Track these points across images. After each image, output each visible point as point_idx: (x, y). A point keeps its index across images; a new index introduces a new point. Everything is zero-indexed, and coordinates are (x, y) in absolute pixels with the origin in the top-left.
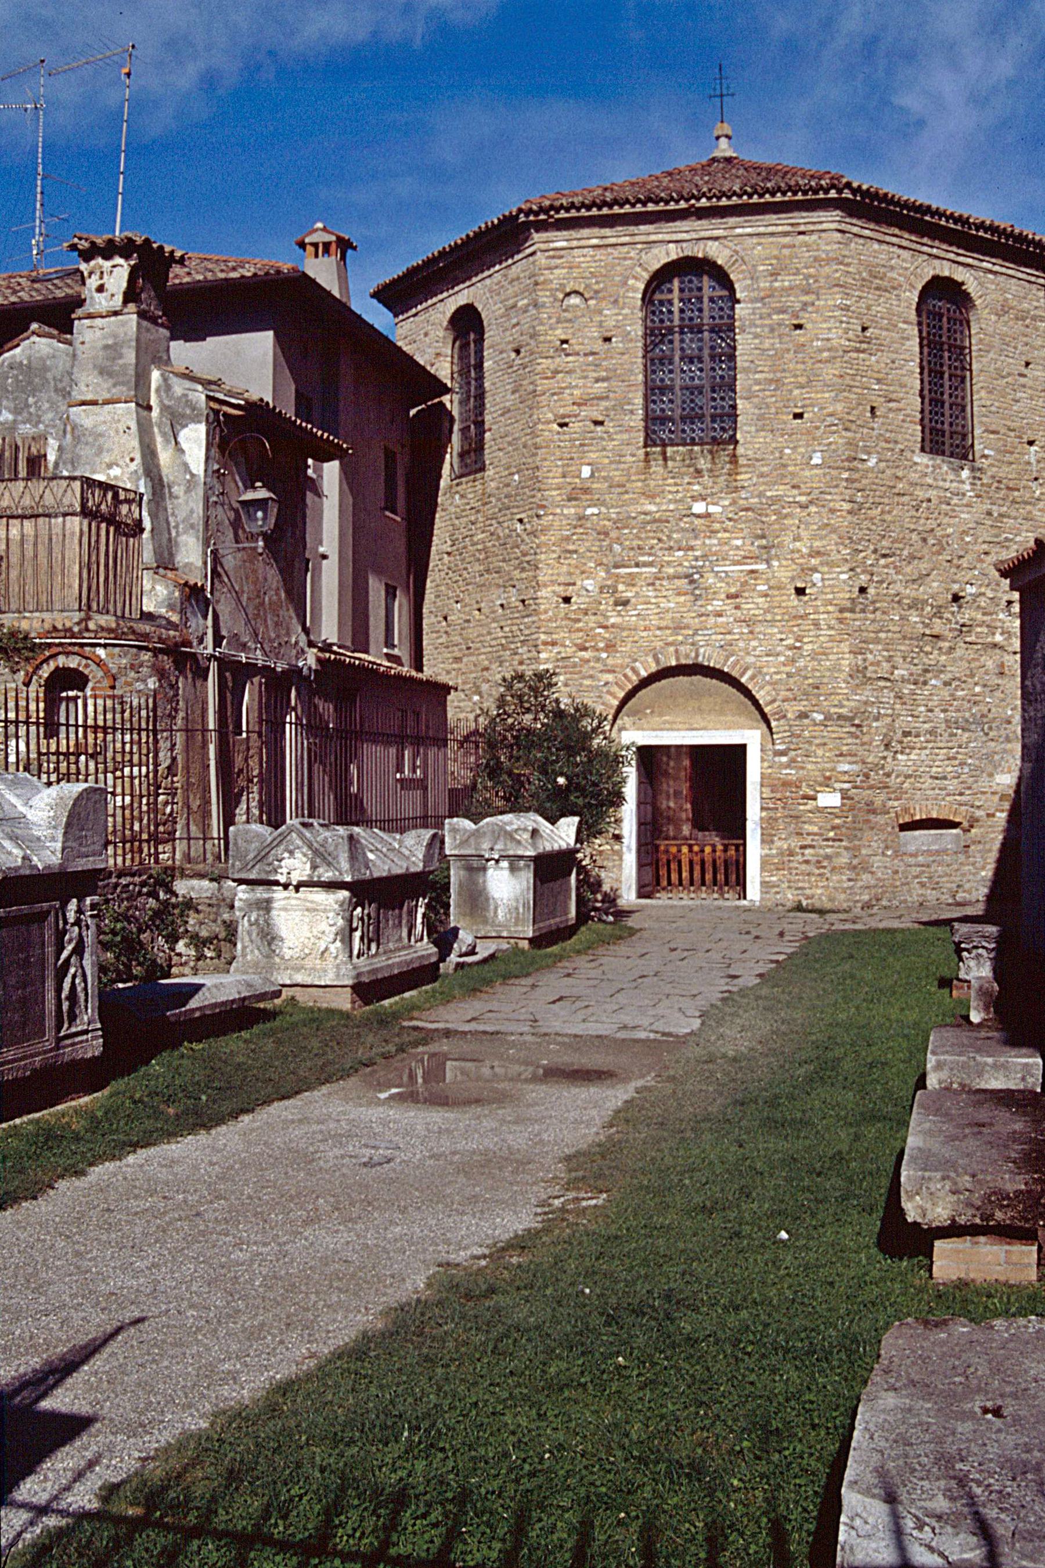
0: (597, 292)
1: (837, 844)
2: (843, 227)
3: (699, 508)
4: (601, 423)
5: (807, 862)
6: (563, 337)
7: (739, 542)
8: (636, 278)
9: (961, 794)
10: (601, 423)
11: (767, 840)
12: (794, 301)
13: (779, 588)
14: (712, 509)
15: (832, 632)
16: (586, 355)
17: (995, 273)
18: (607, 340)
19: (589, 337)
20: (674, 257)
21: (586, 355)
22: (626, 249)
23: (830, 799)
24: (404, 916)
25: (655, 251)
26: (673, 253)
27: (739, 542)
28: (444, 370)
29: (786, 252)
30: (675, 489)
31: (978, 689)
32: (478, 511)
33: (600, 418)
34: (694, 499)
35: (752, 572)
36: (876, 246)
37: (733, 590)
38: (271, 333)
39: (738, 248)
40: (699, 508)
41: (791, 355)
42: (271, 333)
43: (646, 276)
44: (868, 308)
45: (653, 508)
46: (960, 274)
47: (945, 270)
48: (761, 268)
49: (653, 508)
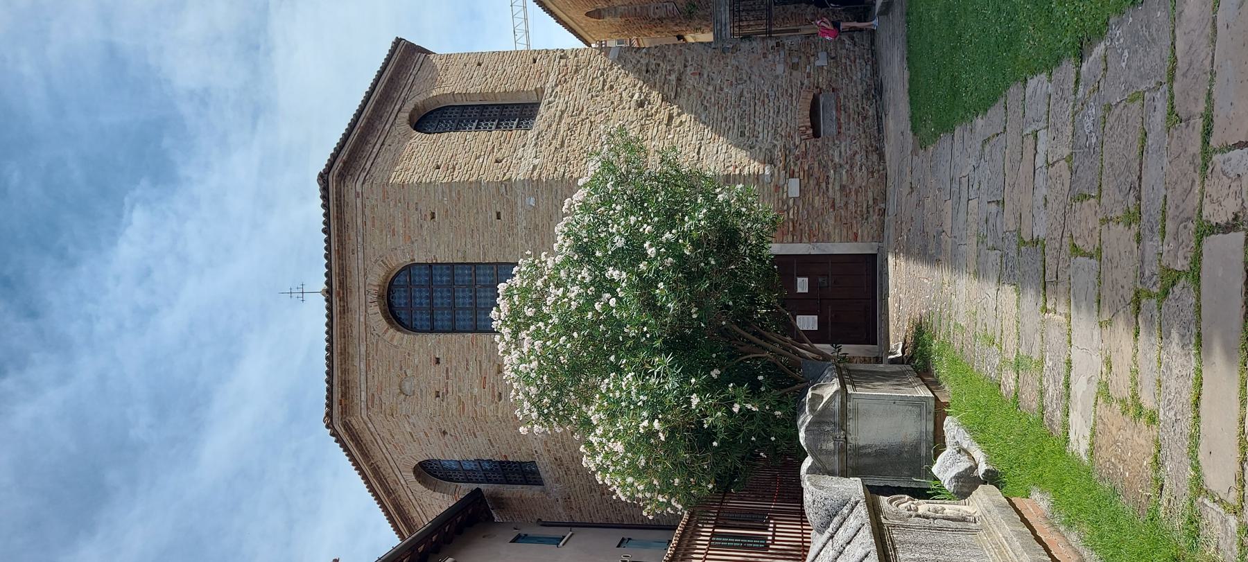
1: (831, 181)
2: (361, 179)
5: (846, 204)
6: (434, 395)
8: (392, 339)
9: (791, 95)
11: (828, 238)
12: (415, 217)
17: (412, 85)
20: (377, 309)
23: (794, 187)
24: (908, 537)
25: (372, 323)
26: (375, 309)
28: (465, 489)
29: (377, 223)
31: (711, 88)
36: (379, 160)
38: (816, 328)
41: (453, 220)
42: (816, 328)
43: (392, 331)
46: (409, 107)
47: (405, 115)
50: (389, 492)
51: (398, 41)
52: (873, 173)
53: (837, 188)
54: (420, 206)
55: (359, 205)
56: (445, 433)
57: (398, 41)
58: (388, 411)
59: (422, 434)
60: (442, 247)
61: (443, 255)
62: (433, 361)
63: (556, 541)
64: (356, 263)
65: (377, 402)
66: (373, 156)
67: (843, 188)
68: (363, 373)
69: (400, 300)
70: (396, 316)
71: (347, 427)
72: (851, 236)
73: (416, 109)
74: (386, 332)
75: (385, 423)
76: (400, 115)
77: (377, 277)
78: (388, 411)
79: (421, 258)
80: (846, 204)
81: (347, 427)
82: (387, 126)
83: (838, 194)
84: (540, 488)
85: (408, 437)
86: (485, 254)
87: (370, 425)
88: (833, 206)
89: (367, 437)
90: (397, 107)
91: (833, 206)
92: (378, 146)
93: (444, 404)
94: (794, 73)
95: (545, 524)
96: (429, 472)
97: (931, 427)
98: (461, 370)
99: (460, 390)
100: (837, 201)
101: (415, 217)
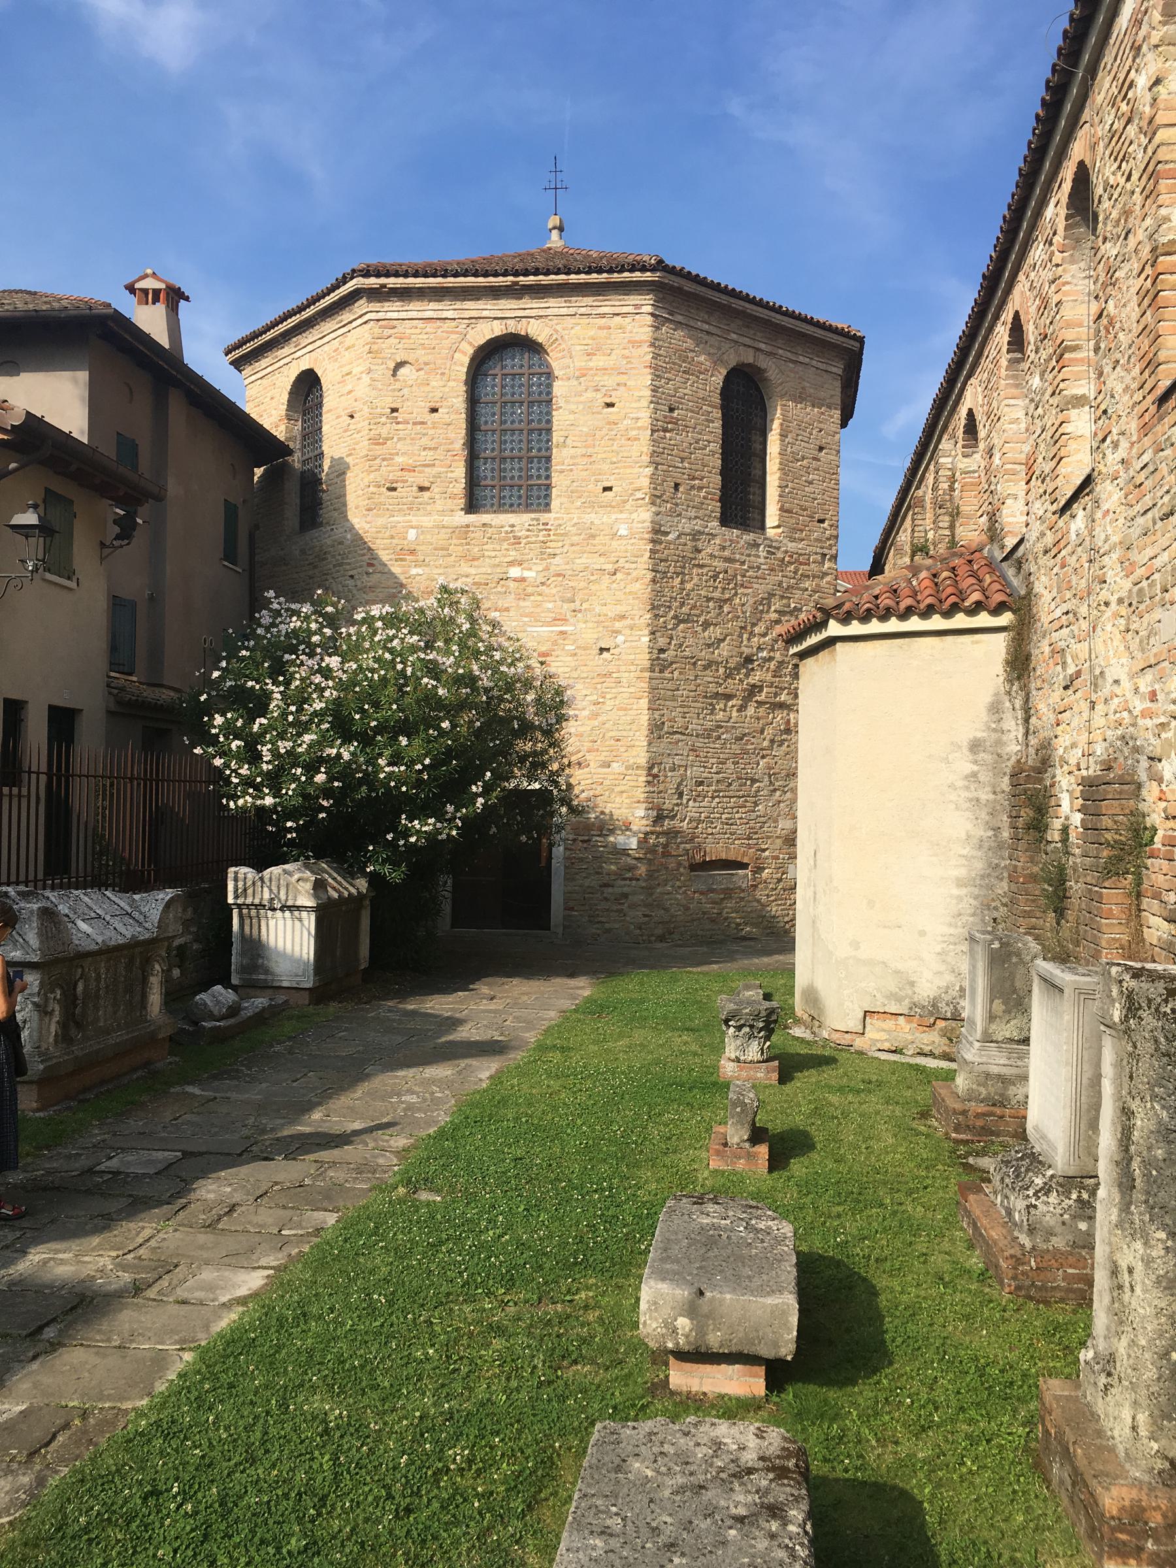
0: (426, 364)
3: (515, 572)
4: (428, 489)
6: (393, 406)
7: (550, 605)
10: (428, 489)
12: (610, 381)
13: (585, 649)
14: (526, 574)
15: (632, 690)
16: (414, 424)
18: (434, 410)
19: (415, 408)
20: (498, 333)
21: (414, 424)
22: (454, 324)
26: (497, 329)
27: (550, 605)
30: (493, 554)
32: (315, 567)
33: (427, 484)
34: (511, 563)
35: (562, 633)
37: (544, 649)
39: (558, 328)
40: (515, 572)
43: (472, 351)
44: (676, 391)
45: (473, 571)
46: (763, 362)
47: (748, 357)
48: (578, 348)
49: (473, 571)
50: (286, 336)
51: (861, 340)
52: (640, 928)
53: (626, 890)
54: (622, 388)
55: (625, 310)
56: (352, 417)
57: (861, 340)
58: (375, 347)
59: (350, 387)
60: (572, 417)
61: (560, 419)
62: (433, 405)
63: (230, 554)
64: (555, 305)
65: (387, 332)
66: (692, 323)
67: (625, 896)
68: (420, 315)
69: (515, 362)
70: (488, 355)
71: (355, 295)
72: (571, 904)
73: (760, 371)
74: (470, 344)
75: (362, 342)
76: (751, 352)
77: (536, 330)
78: (375, 347)
79: (558, 388)
80: (606, 899)
81: (355, 295)
82: (734, 336)
83: (619, 890)
84: (297, 528)
85: (346, 370)
86: (562, 472)
87: (360, 321)
88: (606, 885)
89: (346, 316)
90: (763, 346)
91: (606, 885)
92: (706, 327)
93: (384, 419)
94: (779, 841)
95: (251, 537)
96: (307, 388)
97: (285, 984)
98: (425, 441)
99: (399, 439)
100: (610, 890)
101: (610, 381)
